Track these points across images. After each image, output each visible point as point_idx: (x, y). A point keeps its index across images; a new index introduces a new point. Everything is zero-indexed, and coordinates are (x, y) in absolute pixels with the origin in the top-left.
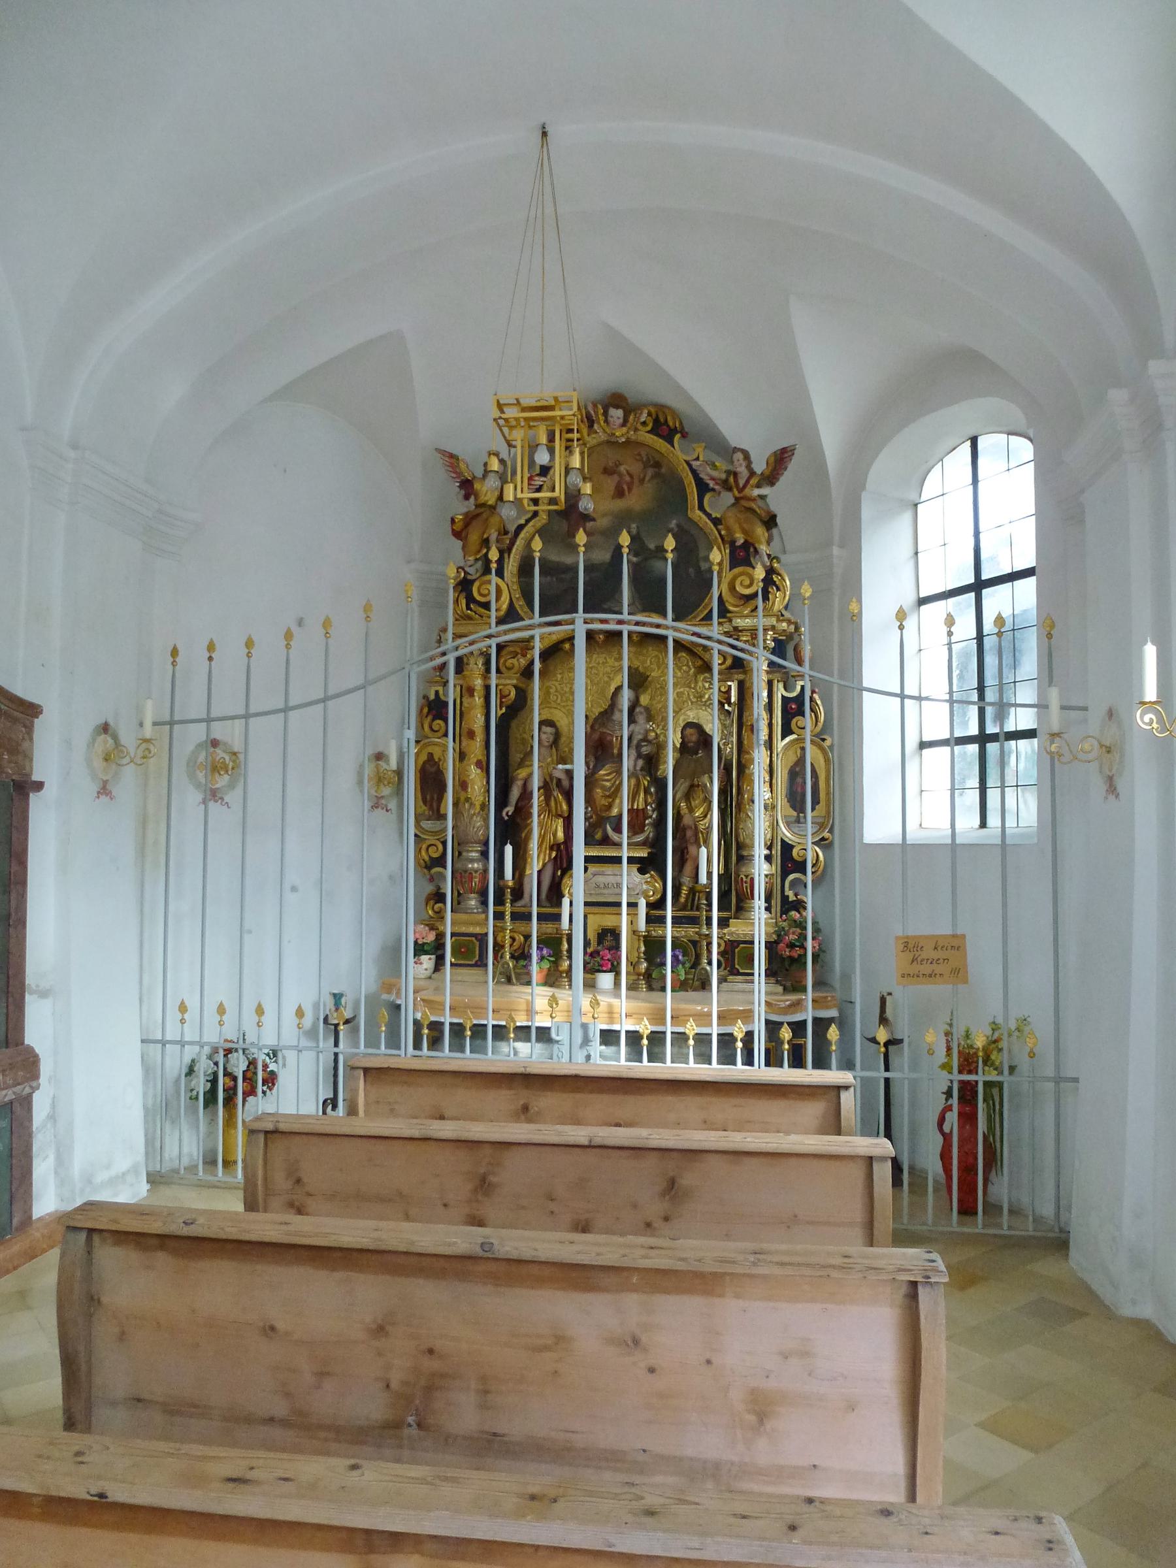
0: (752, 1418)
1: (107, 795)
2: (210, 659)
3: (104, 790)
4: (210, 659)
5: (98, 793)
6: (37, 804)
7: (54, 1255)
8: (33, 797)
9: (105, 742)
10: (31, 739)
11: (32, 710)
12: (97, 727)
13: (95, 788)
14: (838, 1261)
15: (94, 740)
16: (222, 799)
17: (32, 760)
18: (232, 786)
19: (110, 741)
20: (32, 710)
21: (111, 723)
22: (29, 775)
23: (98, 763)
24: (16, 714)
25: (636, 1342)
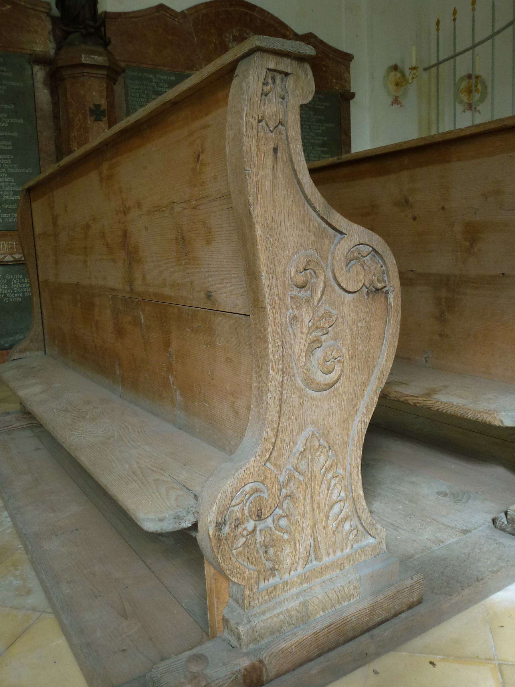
0: (466, 243)
1: (398, 104)
2: (455, 19)
3: (396, 101)
4: (455, 19)
5: (392, 102)
6: (354, 106)
7: (12, 259)
8: (353, 103)
9: (395, 76)
10: (349, 72)
11: (348, 58)
12: (390, 67)
13: (390, 100)
14: (277, 297)
15: (388, 75)
16: (475, 108)
17: (350, 83)
18: (482, 100)
19: (399, 75)
20: (348, 58)
21: (399, 64)
22: (350, 91)
23: (392, 87)
24: (339, 59)
25: (407, 201)
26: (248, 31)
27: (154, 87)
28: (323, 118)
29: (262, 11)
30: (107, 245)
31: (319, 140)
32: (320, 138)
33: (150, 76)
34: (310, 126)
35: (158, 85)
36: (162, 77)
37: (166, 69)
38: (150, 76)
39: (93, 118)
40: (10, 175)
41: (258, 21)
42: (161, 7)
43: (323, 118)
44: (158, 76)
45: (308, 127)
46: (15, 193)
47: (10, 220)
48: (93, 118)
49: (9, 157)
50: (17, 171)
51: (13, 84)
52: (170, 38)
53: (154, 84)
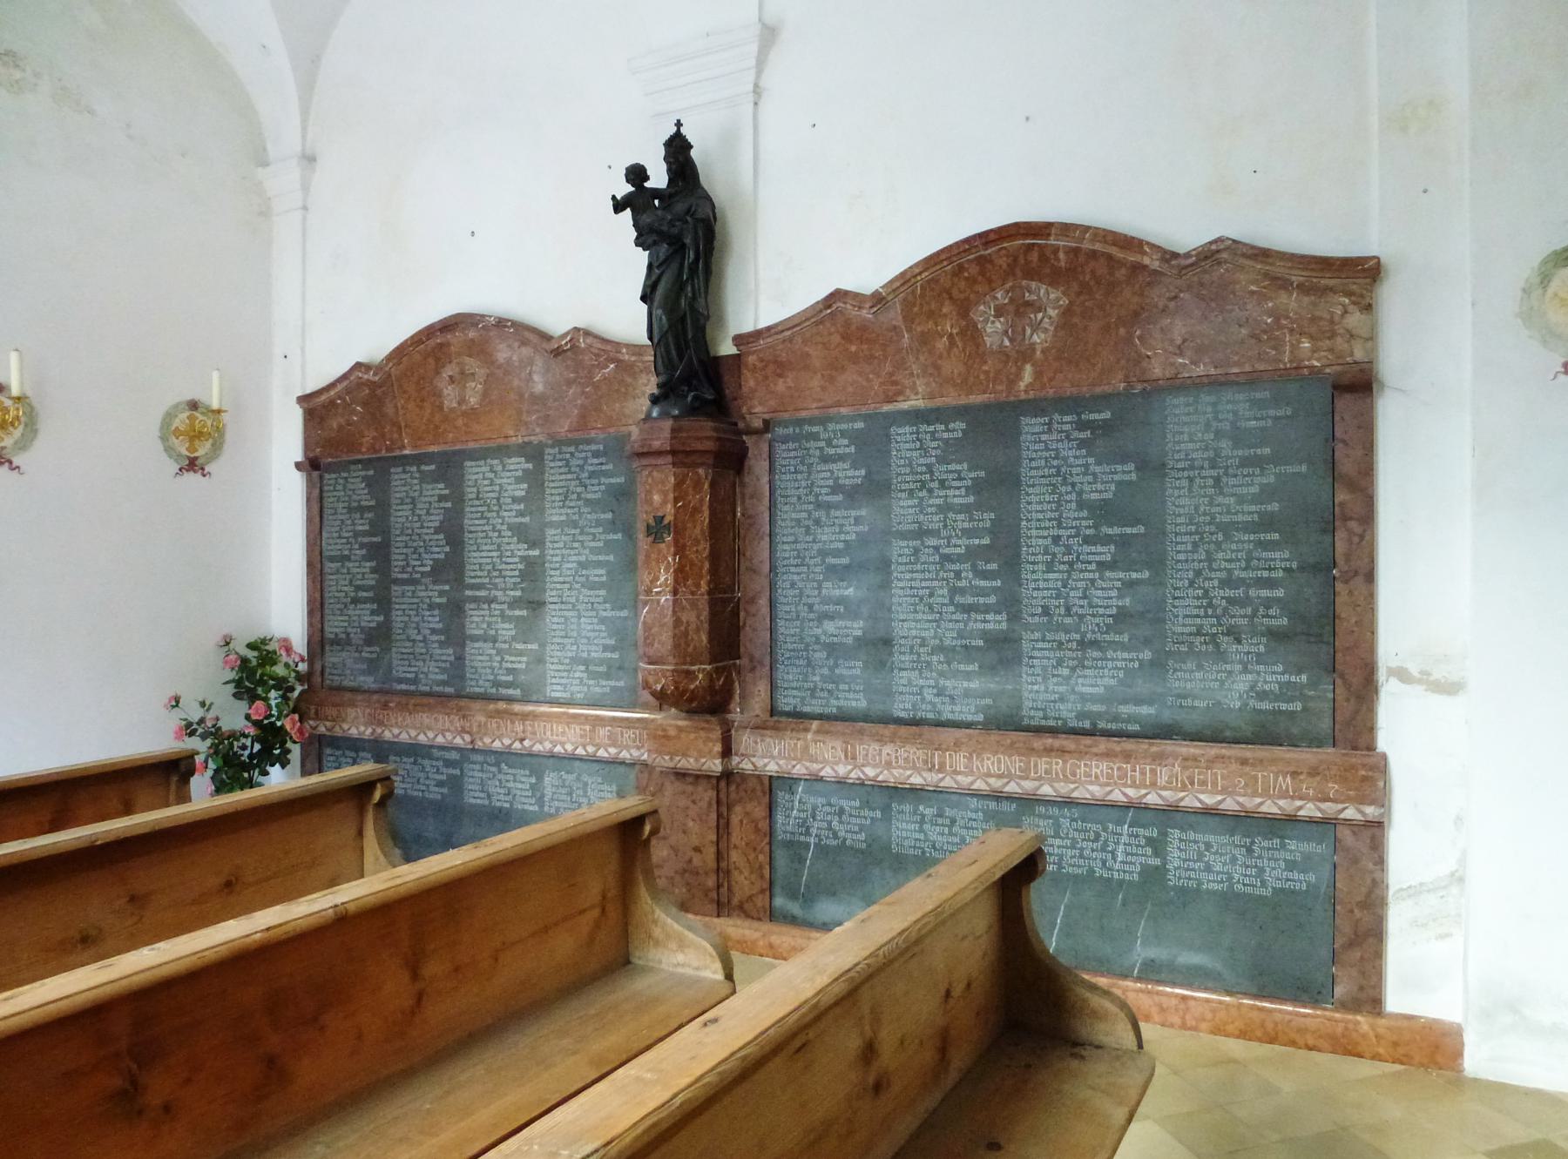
26: (1034, 285)
27: (821, 449)
28: (1276, 536)
29: (1066, 229)
30: (415, 975)
31: (1250, 513)
32: (1253, 508)
33: (815, 429)
34: (1217, 480)
35: (829, 443)
36: (838, 427)
37: (844, 411)
38: (815, 429)
39: (650, 539)
40: (602, 621)
41: (1061, 255)
42: (838, 295)
43: (1276, 536)
44: (831, 426)
45: (1210, 482)
46: (606, 648)
47: (597, 690)
48: (650, 539)
49: (602, 592)
50: (609, 614)
51: (613, 481)
52: (853, 348)
53: (823, 444)
